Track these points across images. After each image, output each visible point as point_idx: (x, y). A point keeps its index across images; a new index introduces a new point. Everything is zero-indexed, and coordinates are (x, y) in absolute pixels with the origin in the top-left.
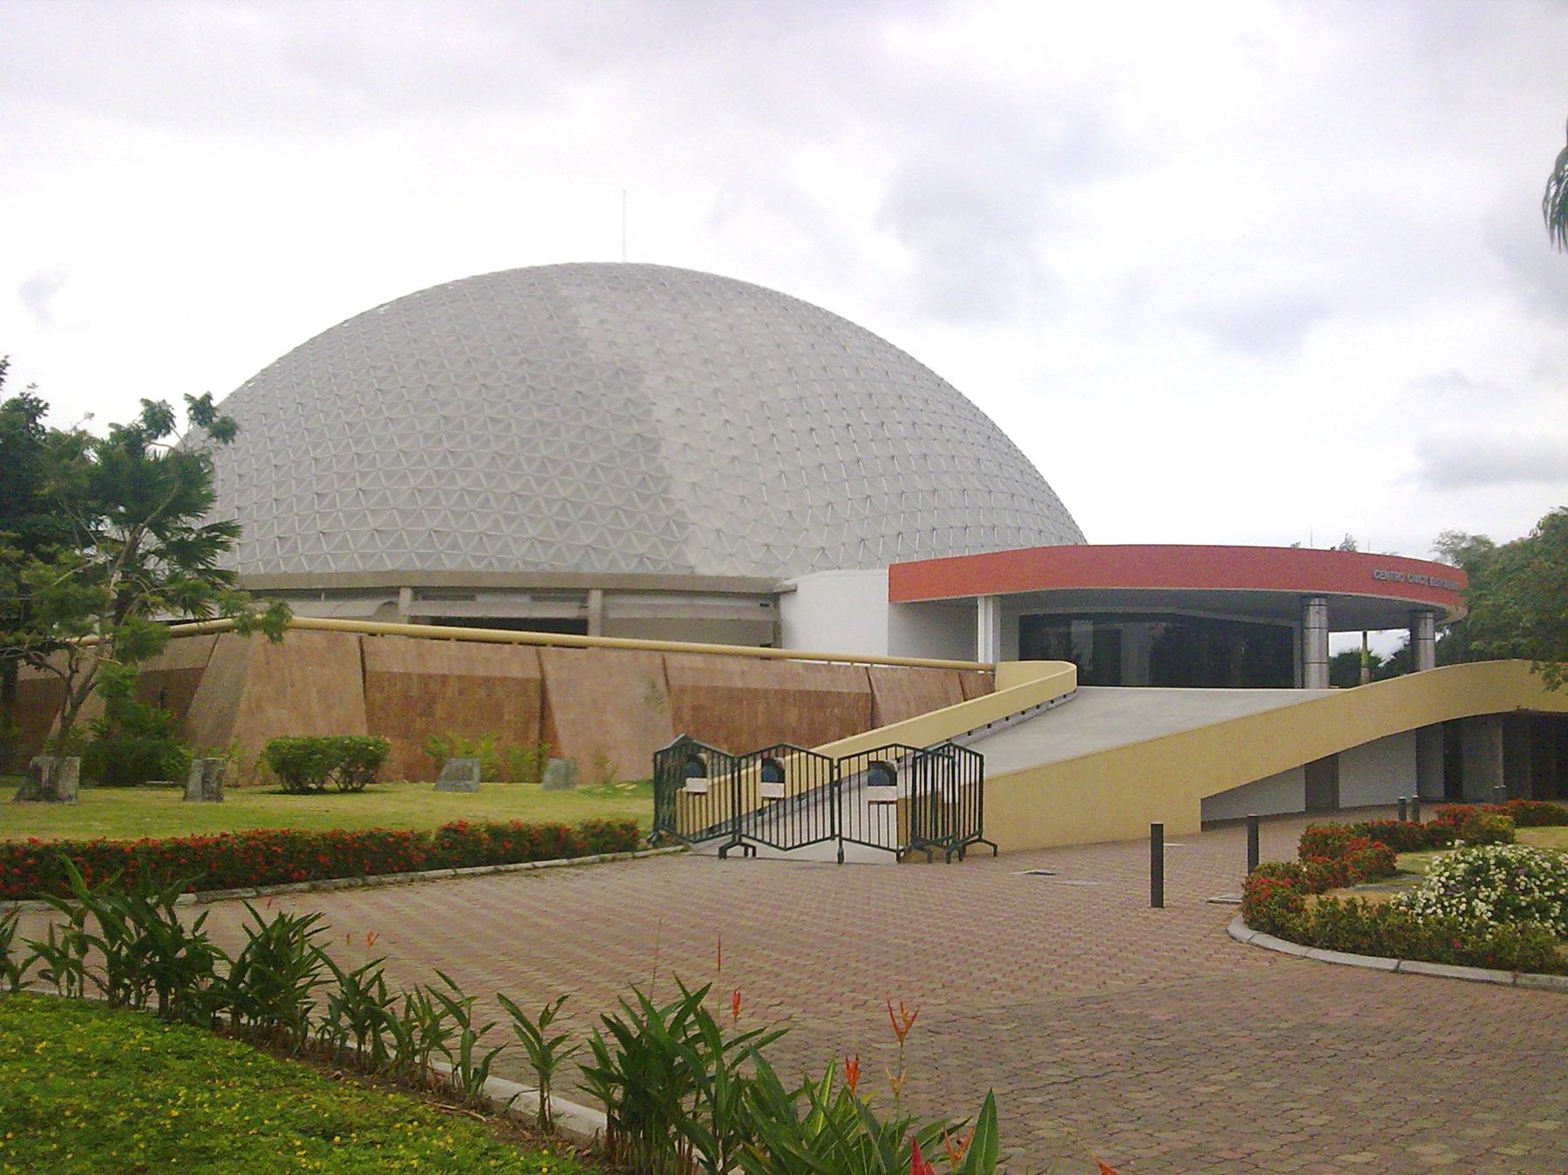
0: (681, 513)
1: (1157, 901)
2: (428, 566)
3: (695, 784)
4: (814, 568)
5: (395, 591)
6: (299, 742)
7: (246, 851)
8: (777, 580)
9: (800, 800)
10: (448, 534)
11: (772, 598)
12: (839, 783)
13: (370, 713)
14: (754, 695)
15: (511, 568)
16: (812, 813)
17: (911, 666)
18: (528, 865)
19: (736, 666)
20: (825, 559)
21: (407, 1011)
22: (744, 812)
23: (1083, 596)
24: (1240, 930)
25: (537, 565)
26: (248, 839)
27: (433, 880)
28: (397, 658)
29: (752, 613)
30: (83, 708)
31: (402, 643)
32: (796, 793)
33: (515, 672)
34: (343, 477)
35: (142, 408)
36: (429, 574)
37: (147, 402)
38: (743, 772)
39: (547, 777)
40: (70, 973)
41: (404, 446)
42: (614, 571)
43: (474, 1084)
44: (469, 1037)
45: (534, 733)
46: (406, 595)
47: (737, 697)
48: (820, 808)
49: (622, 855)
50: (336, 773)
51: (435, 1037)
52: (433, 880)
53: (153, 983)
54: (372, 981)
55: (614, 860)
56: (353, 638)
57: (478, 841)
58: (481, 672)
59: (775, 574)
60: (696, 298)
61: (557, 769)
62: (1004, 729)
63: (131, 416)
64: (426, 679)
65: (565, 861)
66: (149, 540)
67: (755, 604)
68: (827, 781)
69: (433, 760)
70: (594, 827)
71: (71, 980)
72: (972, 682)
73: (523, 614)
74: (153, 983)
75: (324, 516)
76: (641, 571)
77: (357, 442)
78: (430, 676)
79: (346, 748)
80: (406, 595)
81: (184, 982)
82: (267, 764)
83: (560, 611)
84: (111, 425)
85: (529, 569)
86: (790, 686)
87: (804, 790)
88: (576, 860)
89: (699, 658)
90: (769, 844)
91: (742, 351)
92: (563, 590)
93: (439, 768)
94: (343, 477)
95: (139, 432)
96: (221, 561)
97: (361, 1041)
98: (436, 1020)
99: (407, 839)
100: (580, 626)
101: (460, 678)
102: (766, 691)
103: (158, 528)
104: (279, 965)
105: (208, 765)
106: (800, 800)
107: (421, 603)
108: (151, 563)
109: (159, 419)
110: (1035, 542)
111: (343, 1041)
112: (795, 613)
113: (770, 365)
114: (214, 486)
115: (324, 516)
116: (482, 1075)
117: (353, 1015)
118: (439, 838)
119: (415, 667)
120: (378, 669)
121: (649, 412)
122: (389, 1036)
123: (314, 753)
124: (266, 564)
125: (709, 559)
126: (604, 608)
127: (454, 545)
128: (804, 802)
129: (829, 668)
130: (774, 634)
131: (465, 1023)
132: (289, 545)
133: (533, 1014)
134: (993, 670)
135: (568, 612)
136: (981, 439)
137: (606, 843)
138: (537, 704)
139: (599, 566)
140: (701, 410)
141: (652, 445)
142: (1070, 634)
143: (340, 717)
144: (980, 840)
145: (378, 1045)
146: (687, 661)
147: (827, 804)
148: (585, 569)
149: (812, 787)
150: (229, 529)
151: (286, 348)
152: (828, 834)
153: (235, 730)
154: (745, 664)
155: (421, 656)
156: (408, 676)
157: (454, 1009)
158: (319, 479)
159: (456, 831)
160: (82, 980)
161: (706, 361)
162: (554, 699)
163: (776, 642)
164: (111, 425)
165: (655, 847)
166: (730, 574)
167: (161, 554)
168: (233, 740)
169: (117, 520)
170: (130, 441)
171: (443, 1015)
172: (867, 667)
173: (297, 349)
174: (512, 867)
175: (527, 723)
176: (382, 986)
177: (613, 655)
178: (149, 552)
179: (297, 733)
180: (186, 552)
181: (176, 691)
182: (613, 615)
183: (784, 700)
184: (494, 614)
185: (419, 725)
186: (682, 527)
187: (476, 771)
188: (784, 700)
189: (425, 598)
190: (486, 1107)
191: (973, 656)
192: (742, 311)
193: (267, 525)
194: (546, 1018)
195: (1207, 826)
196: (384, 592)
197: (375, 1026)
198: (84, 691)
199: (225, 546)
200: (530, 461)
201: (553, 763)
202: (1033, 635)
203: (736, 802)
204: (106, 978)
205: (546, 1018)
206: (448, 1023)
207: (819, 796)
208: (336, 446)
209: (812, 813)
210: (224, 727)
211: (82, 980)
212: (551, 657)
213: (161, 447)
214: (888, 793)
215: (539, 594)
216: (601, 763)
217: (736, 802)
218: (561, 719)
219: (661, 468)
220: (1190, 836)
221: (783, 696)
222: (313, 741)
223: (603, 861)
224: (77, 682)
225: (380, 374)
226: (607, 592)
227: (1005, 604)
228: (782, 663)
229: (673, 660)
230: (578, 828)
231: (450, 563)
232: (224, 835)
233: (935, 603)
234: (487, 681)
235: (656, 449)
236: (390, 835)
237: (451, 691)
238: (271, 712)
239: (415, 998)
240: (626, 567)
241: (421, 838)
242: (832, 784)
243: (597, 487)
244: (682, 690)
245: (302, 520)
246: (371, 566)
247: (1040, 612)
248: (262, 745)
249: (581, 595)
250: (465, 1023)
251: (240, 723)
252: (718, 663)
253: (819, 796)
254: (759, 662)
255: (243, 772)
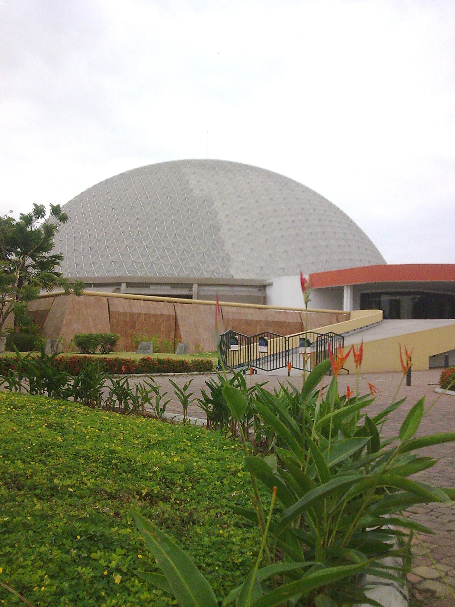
0: (228, 255)
1: (409, 383)
2: (132, 275)
3: (234, 347)
4: (279, 276)
5: (120, 284)
6: (86, 335)
7: (71, 362)
8: (265, 280)
9: (274, 356)
10: (139, 263)
11: (263, 287)
12: (288, 351)
13: (112, 326)
14: (257, 323)
15: (163, 276)
16: (278, 361)
17: (317, 312)
18: (172, 374)
19: (249, 312)
20: (284, 272)
21: (137, 392)
22: (252, 359)
23: (386, 285)
24: (439, 390)
25: (173, 274)
26: (72, 358)
27: (138, 377)
28: (121, 307)
29: (255, 292)
30: (7, 319)
31: (123, 301)
32: (272, 354)
33: (166, 312)
34: (100, 241)
35: (33, 207)
36: (132, 278)
37: (35, 205)
38: (252, 345)
39: (178, 350)
40: (16, 387)
41: (123, 229)
42: (203, 277)
43: (160, 414)
44: (158, 397)
45: (172, 336)
46: (124, 286)
47: (248, 323)
48: (281, 359)
49: (207, 372)
50: (99, 347)
51: (147, 399)
52: (138, 377)
53: (46, 389)
54: (124, 383)
55: (204, 374)
56: (105, 299)
57: (154, 364)
58: (153, 312)
59: (265, 278)
60: (235, 172)
61: (181, 347)
62: (353, 334)
63: (29, 210)
64: (132, 315)
65: (186, 373)
66: (29, 261)
67: (257, 290)
68: (284, 350)
69: (134, 344)
70: (196, 362)
71: (16, 389)
72: (340, 317)
73: (168, 293)
74: (46, 389)
75: (93, 256)
76: (213, 277)
77: (105, 228)
78: (133, 313)
79: (103, 337)
80: (124, 286)
81: (57, 387)
82: (74, 343)
83: (183, 289)
84: (21, 214)
85: (170, 276)
86: (270, 319)
87: (275, 353)
88: (190, 373)
89: (235, 308)
90: (262, 369)
91: (252, 192)
92: (184, 284)
93: (137, 348)
94: (100, 241)
95: (31, 217)
96: (57, 269)
97: (120, 403)
98: (147, 393)
99: (128, 362)
100: (190, 297)
101: (145, 314)
102: (261, 321)
103: (33, 257)
104: (91, 379)
105: (53, 342)
106: (274, 356)
107: (129, 288)
108: (30, 269)
109: (39, 211)
110: (366, 264)
111: (114, 405)
112: (271, 292)
113: (263, 197)
114: (53, 240)
115: (93, 256)
116: (163, 410)
117: (117, 394)
118: (139, 362)
119: (128, 310)
120: (115, 310)
121: (216, 216)
122: (130, 402)
123: (91, 339)
124: (71, 274)
125: (238, 272)
126: (198, 291)
127: (142, 267)
128: (275, 357)
129: (285, 313)
130: (264, 300)
131: (157, 393)
132: (79, 267)
133: (181, 387)
134: (349, 314)
135: (185, 292)
136: (346, 226)
137: (201, 368)
138: (174, 324)
139: (197, 275)
140: (236, 215)
141: (217, 229)
142: (380, 301)
143: (101, 327)
144: (342, 368)
145: (126, 404)
146: (230, 309)
147: (284, 358)
148: (191, 276)
149: (278, 352)
150: (59, 257)
151: (78, 193)
152: (284, 365)
153: (62, 332)
154: (252, 311)
155: (130, 306)
156: (126, 313)
157: (154, 389)
158: (91, 242)
159: (146, 360)
160: (20, 389)
161: (238, 196)
162: (179, 323)
163: (265, 303)
164: (21, 214)
165: (219, 370)
166: (247, 278)
167: (34, 267)
168: (61, 336)
169: (17, 254)
170: (28, 220)
171: (150, 392)
172: (299, 313)
173: (82, 193)
174: (166, 374)
175: (169, 332)
176: (128, 384)
177: (202, 307)
178: (29, 266)
179: (84, 332)
180: (43, 266)
181: (41, 316)
182: (201, 293)
183: (267, 325)
184: (155, 293)
185: (130, 331)
186: (228, 260)
187: (151, 347)
188: (267, 325)
189: (131, 287)
190: (164, 420)
191: (341, 308)
192: (252, 177)
193: (74, 258)
194: (186, 387)
195: (430, 368)
196: (116, 285)
197: (125, 398)
198: (7, 313)
199: (58, 264)
200: (170, 235)
201: (180, 345)
202: (366, 300)
203: (249, 356)
204: (29, 388)
205: (186, 387)
206: (152, 394)
207: (281, 355)
208: (97, 230)
209: (278, 361)
210: (58, 330)
211: (20, 389)
212: (179, 307)
213: (38, 224)
214: (308, 350)
215: (175, 285)
216: (197, 347)
217: (249, 356)
218: (182, 330)
219: (221, 238)
220: (426, 370)
221: (267, 323)
222: (91, 335)
223: (200, 374)
224: (4, 311)
225: (113, 202)
226: (199, 285)
227: (355, 289)
228: (267, 311)
229: (225, 309)
230: (190, 361)
231: (141, 274)
232: (63, 357)
233: (326, 288)
234: (154, 316)
235: (219, 230)
236: (122, 360)
237: (142, 318)
238: (75, 326)
239: (139, 386)
240: (206, 275)
241: (134, 361)
242: (286, 351)
243: (196, 245)
244: (228, 320)
245: (85, 257)
246: (111, 274)
247: (369, 292)
248: (72, 337)
249: (189, 286)
250: (157, 393)
251: (63, 330)
252: (242, 310)
253: (281, 355)
254: (257, 310)
255: (65, 348)
